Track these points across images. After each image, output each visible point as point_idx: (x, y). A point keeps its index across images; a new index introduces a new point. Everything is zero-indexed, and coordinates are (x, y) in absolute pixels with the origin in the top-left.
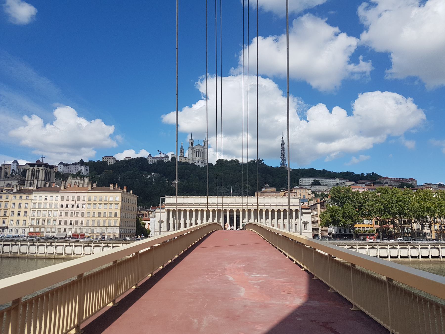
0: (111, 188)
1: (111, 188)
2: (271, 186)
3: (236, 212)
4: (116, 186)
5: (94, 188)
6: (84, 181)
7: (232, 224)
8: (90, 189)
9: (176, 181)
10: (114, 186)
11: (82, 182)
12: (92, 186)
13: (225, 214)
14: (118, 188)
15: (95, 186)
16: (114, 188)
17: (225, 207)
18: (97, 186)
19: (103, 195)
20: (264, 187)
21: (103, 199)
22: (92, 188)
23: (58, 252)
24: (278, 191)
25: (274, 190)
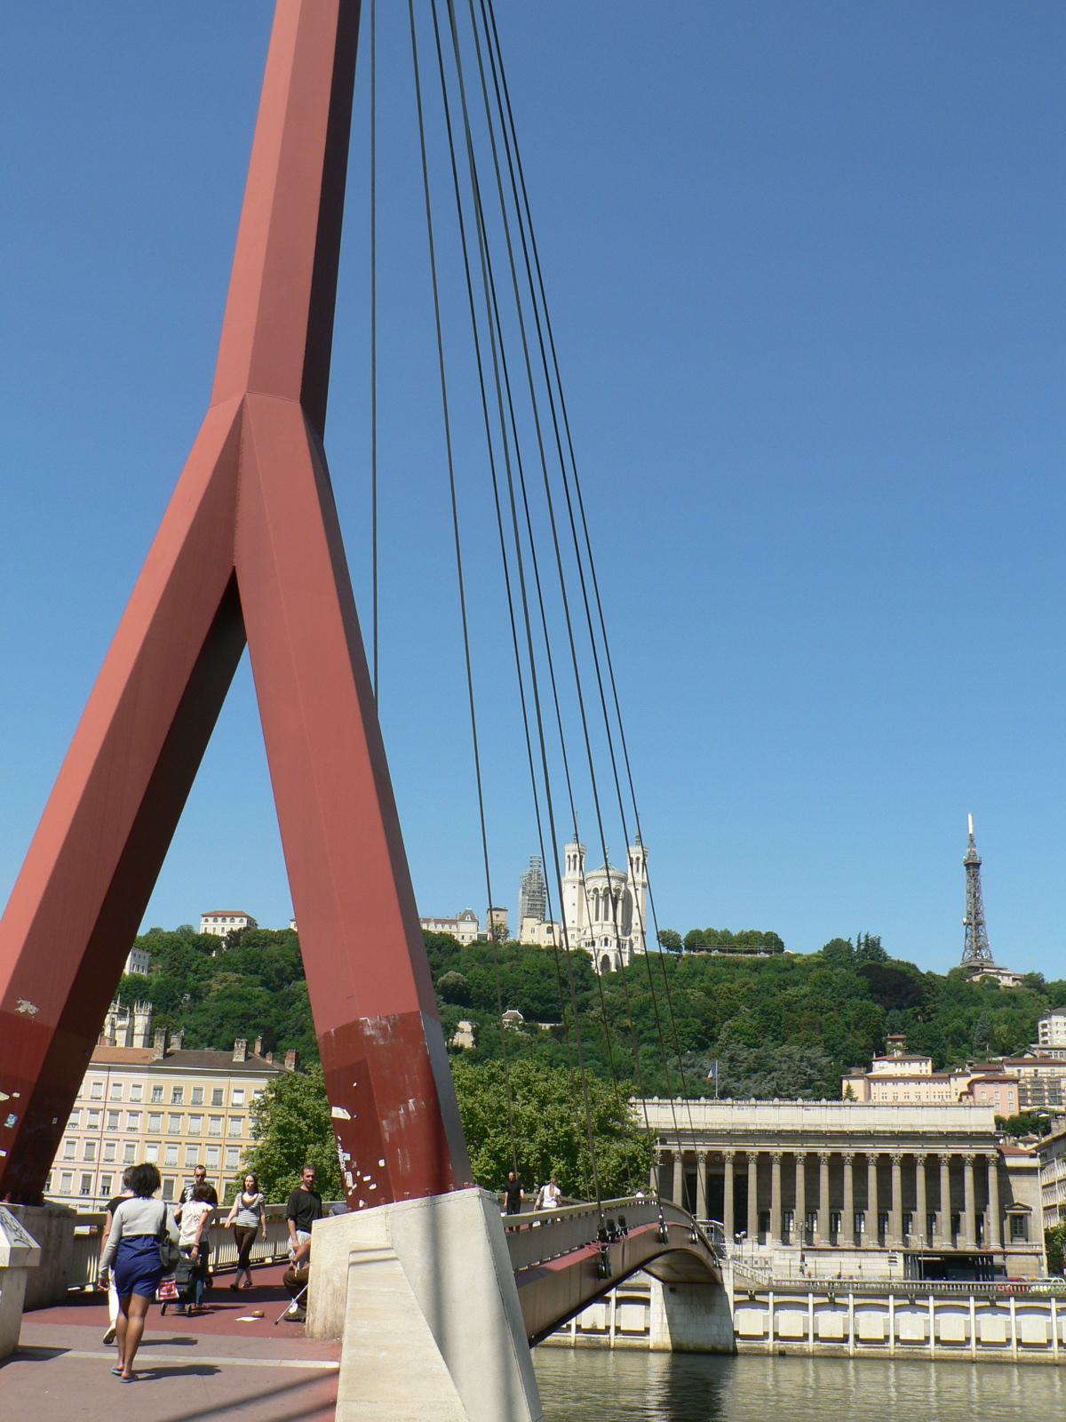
0: (239, 1057)
1: (239, 1057)
2: (914, 1050)
3: (735, 1165)
4: (258, 1048)
5: (170, 1055)
6: (132, 1017)
7: (715, 1211)
8: (159, 1056)
9: (408, 1166)
10: (249, 1048)
11: (125, 1022)
12: (167, 1045)
13: (691, 1171)
14: (263, 1054)
15: (176, 1045)
16: (247, 1058)
17: (687, 1146)
18: (184, 1043)
19: (209, 1084)
20: (882, 1052)
21: (207, 1097)
22: (166, 1055)
23: (878, 1316)
24: (943, 1068)
25: (926, 1068)
